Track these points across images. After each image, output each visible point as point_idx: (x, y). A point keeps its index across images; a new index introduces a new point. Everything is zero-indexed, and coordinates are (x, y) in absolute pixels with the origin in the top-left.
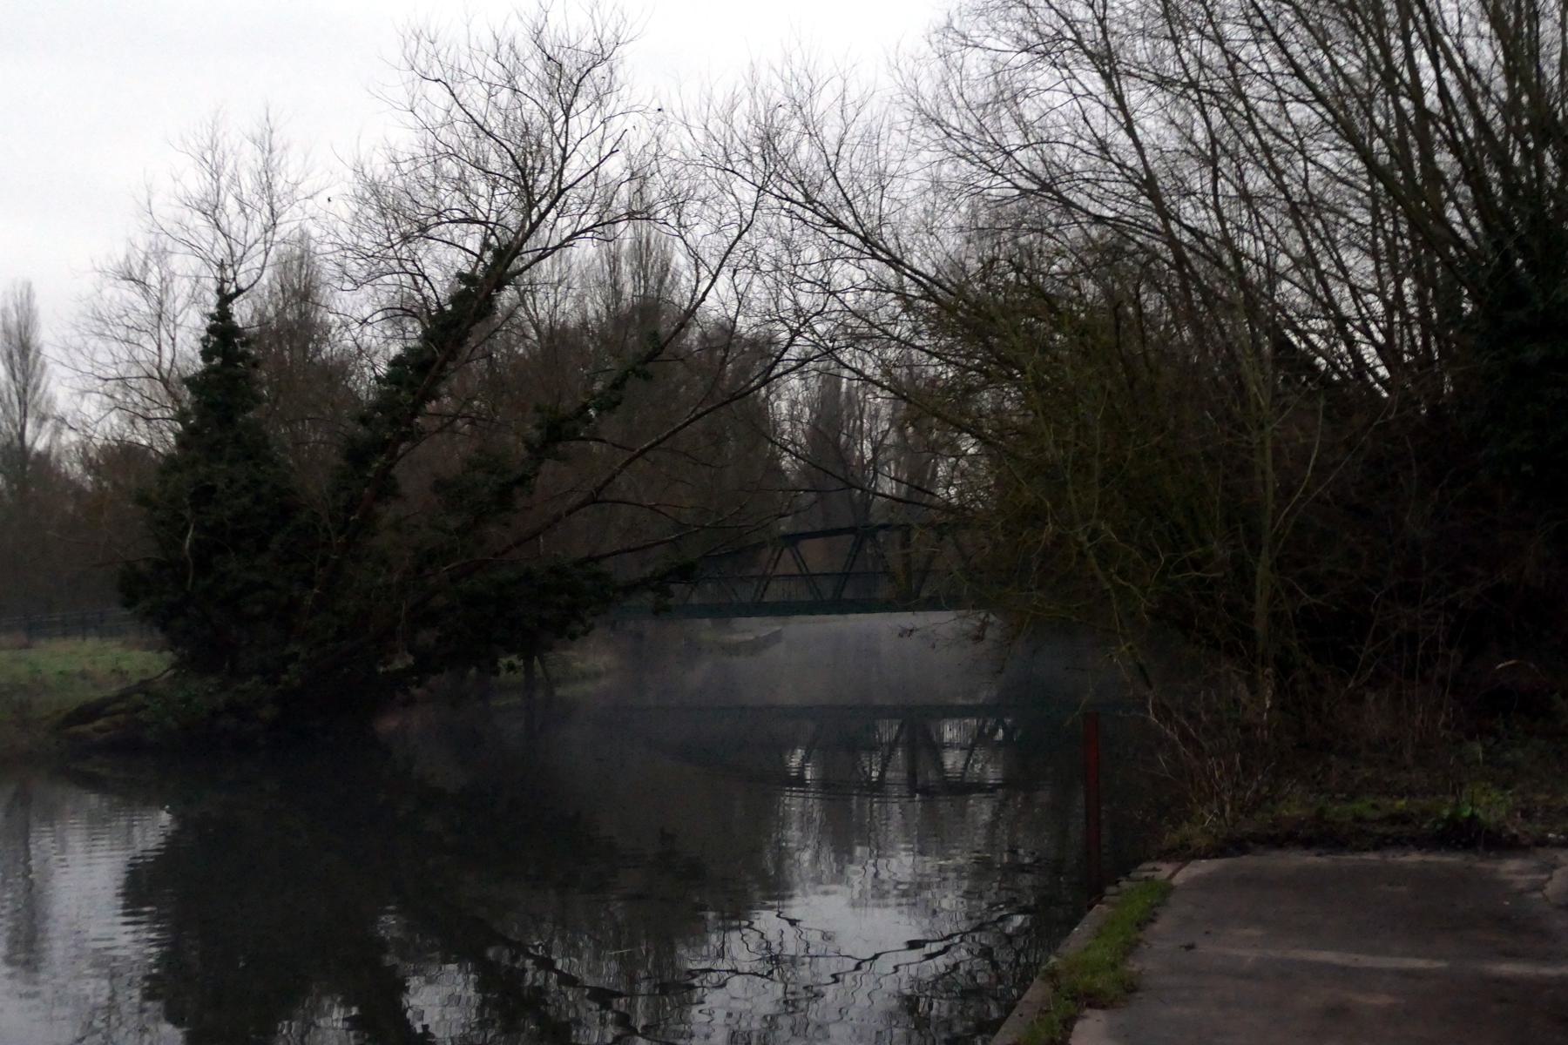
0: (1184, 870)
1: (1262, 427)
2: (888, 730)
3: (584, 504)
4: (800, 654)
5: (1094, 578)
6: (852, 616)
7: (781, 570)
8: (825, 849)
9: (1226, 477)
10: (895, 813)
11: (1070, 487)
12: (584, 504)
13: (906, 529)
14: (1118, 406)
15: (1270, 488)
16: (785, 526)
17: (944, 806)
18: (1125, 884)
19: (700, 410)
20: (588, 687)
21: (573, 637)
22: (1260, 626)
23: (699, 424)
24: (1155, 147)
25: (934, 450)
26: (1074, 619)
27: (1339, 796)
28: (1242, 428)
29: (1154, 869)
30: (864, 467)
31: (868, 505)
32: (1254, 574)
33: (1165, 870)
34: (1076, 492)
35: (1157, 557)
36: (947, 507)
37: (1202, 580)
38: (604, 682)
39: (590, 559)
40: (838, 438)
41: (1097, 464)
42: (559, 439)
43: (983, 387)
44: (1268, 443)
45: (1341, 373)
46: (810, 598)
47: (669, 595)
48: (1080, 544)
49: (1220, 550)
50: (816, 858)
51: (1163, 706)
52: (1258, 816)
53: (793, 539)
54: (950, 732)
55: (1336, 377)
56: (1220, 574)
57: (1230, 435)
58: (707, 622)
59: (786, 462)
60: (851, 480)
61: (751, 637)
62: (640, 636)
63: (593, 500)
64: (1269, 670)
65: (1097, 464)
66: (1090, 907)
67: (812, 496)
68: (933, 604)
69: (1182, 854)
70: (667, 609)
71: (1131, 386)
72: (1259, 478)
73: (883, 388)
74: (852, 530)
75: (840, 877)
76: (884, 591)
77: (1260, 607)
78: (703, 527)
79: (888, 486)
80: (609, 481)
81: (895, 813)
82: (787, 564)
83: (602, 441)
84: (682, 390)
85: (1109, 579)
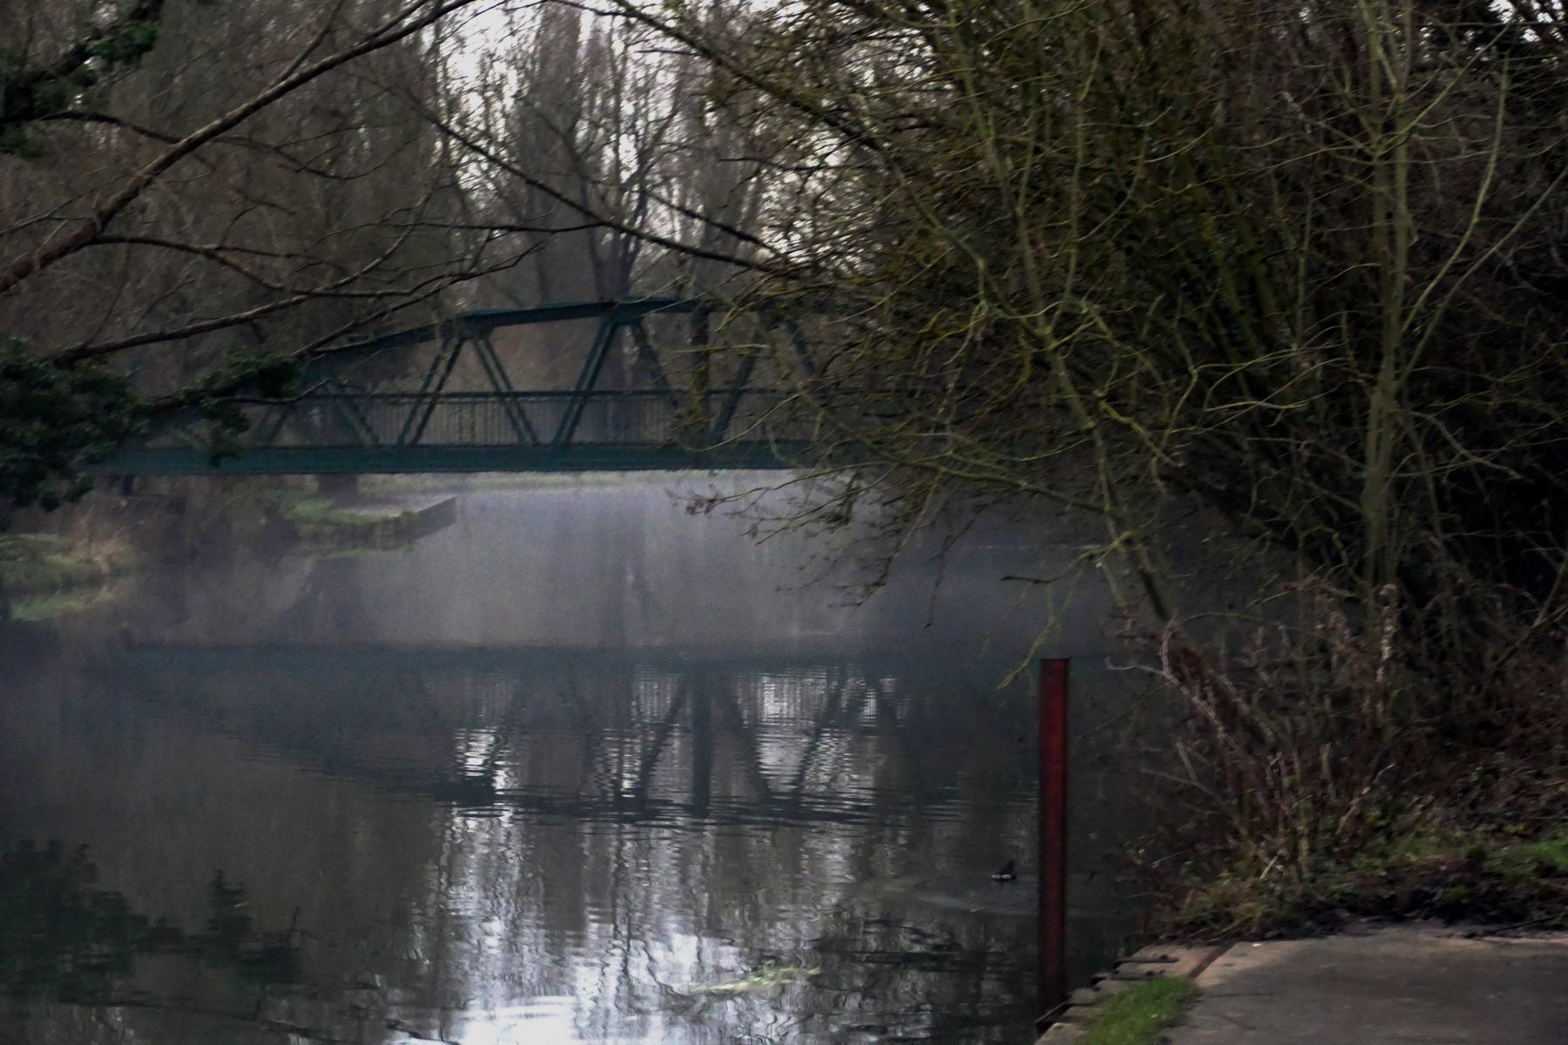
0: (1220, 961)
1: (1389, 127)
2: (653, 698)
3: (75, 245)
4: (497, 547)
5: (1063, 407)
6: (587, 476)
7: (455, 384)
8: (528, 920)
9: (1318, 221)
10: (662, 860)
11: (1023, 232)
12: (75, 245)
13: (703, 311)
14: (1119, 78)
15: (1402, 243)
16: (464, 298)
17: (759, 841)
18: (1109, 985)
19: (306, 67)
20: (75, 603)
21: (50, 504)
22: (1374, 507)
23: (306, 93)
24: (152, 37)
25: (762, 156)
26: (1024, 484)
27: (1511, 828)
28: (1353, 126)
29: (1164, 959)
30: (623, 188)
31: (627, 261)
32: (1364, 407)
33: (1185, 959)
34: (1033, 243)
35: (1182, 370)
36: (781, 269)
37: (1267, 415)
38: (105, 595)
39: (82, 352)
40: (572, 130)
41: (1073, 185)
42: (29, 115)
43: (861, 35)
44: (1402, 157)
45: (1540, 29)
46: (510, 438)
47: (241, 424)
48: (1039, 342)
49: (1305, 361)
50: (511, 943)
51: (1186, 652)
52: (1361, 861)
53: (482, 324)
54: (773, 703)
55: (1530, 36)
56: (1300, 406)
57: (1329, 141)
58: (310, 481)
59: (471, 175)
60: (595, 205)
61: (394, 513)
62: (178, 505)
63: (93, 237)
64: (1390, 587)
65: (1073, 185)
66: (1043, 1028)
67: (518, 241)
68: (755, 456)
69: (1216, 930)
70: (234, 453)
71: (1144, 39)
72: (1380, 222)
73: (668, 32)
74: (603, 308)
75: (555, 982)
76: (656, 428)
77: (1374, 471)
78: (311, 295)
79: (664, 223)
80: (125, 200)
81: (662, 860)
82: (469, 373)
83: (112, 121)
84: (270, 26)
85: (1092, 411)
